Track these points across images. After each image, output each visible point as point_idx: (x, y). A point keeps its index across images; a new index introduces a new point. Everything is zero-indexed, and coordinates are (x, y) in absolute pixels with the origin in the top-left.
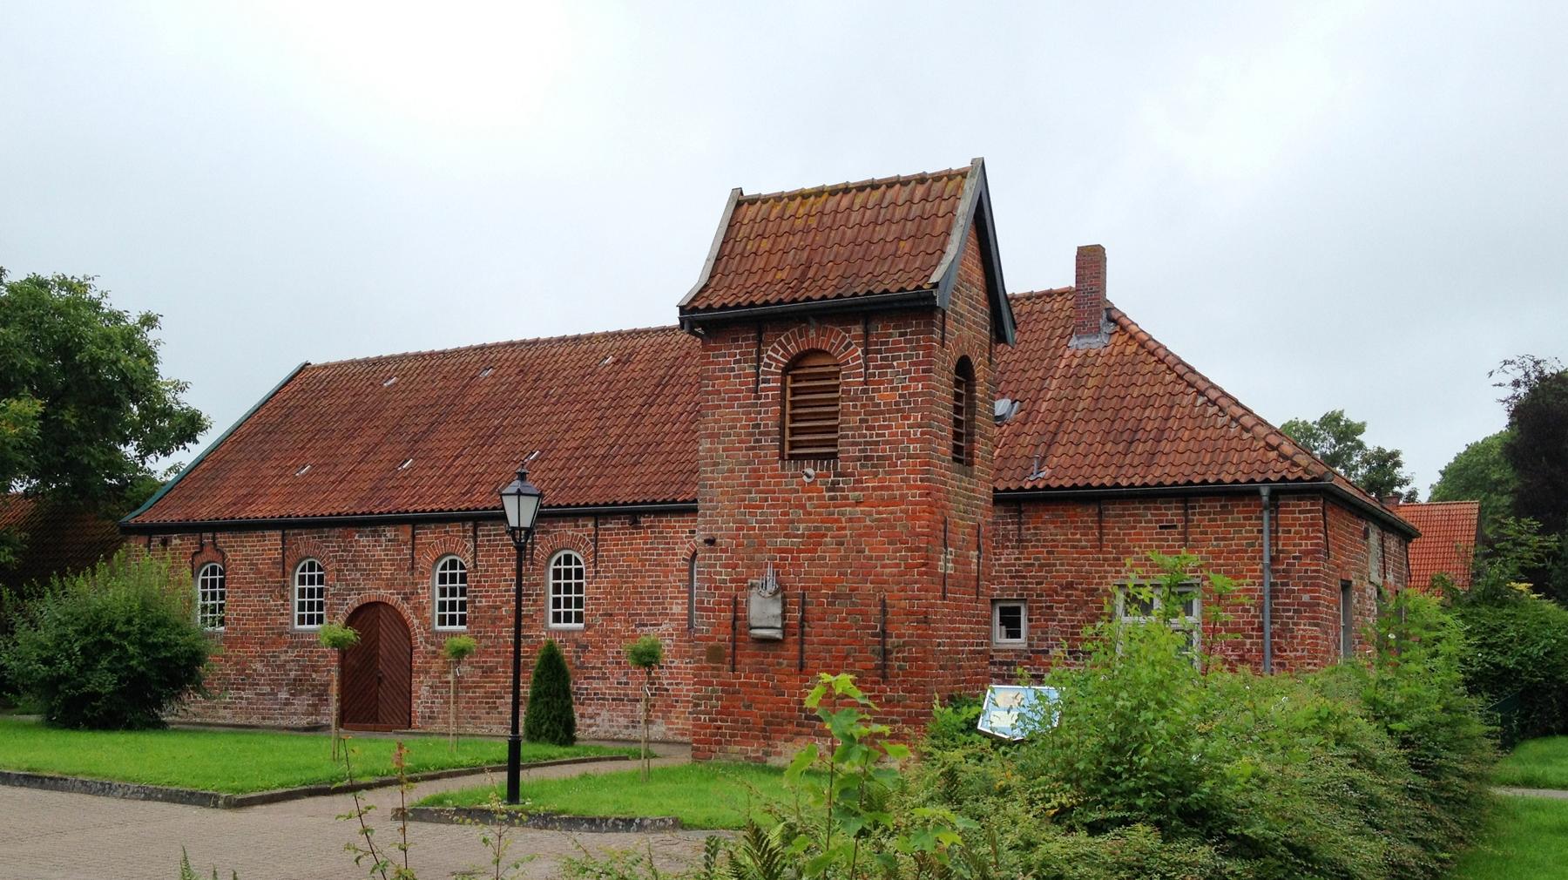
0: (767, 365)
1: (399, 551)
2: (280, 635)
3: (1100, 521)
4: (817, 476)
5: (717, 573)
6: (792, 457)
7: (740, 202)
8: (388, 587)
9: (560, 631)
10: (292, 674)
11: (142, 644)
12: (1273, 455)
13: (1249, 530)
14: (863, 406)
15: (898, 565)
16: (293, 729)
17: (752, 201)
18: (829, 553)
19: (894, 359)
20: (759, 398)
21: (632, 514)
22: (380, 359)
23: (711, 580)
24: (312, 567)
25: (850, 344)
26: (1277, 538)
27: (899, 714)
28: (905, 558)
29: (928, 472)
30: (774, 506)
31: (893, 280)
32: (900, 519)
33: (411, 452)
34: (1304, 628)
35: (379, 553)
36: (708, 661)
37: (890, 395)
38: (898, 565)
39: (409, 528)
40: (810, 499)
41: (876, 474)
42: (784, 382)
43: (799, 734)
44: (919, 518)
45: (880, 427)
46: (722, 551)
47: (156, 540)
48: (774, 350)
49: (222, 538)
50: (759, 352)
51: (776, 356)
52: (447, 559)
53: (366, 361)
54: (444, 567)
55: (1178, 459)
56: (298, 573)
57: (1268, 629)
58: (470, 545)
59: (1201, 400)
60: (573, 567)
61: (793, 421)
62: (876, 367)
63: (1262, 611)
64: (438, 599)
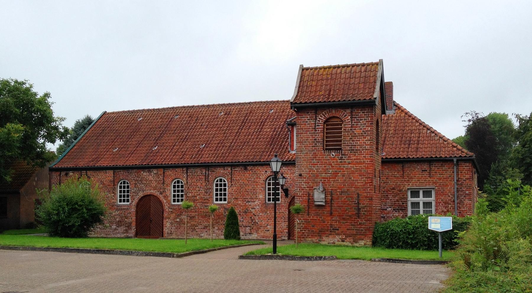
0: (319, 121)
1: (158, 178)
2: (113, 206)
3: (403, 169)
4: (336, 155)
6: (326, 149)
7: (303, 70)
8: (154, 190)
9: (218, 204)
10: (118, 219)
11: (87, 209)
12: (455, 149)
13: (449, 172)
14: (351, 134)
15: (362, 183)
16: (119, 238)
17: (307, 69)
18: (340, 179)
19: (361, 120)
20: (316, 131)
21: (245, 166)
22: (134, 111)
23: (300, 187)
24: (124, 183)
25: (346, 115)
26: (458, 174)
27: (363, 228)
28: (365, 180)
29: (372, 154)
30: (321, 164)
31: (360, 96)
32: (363, 169)
33: (156, 144)
34: (467, 201)
35: (150, 178)
37: (357, 130)
38: (362, 183)
39: (162, 170)
40: (333, 162)
41: (355, 155)
42: (324, 126)
43: (330, 234)
44: (370, 168)
45: (356, 141)
47: (63, 173)
48: (321, 116)
49: (89, 173)
50: (316, 117)
51: (321, 118)
52: (176, 180)
53: (129, 111)
54: (175, 183)
55: (426, 150)
56: (119, 185)
57: (456, 201)
58: (185, 175)
59: (428, 132)
60: (223, 183)
61: (326, 138)
62: (355, 122)
63: (454, 196)
64: (173, 193)
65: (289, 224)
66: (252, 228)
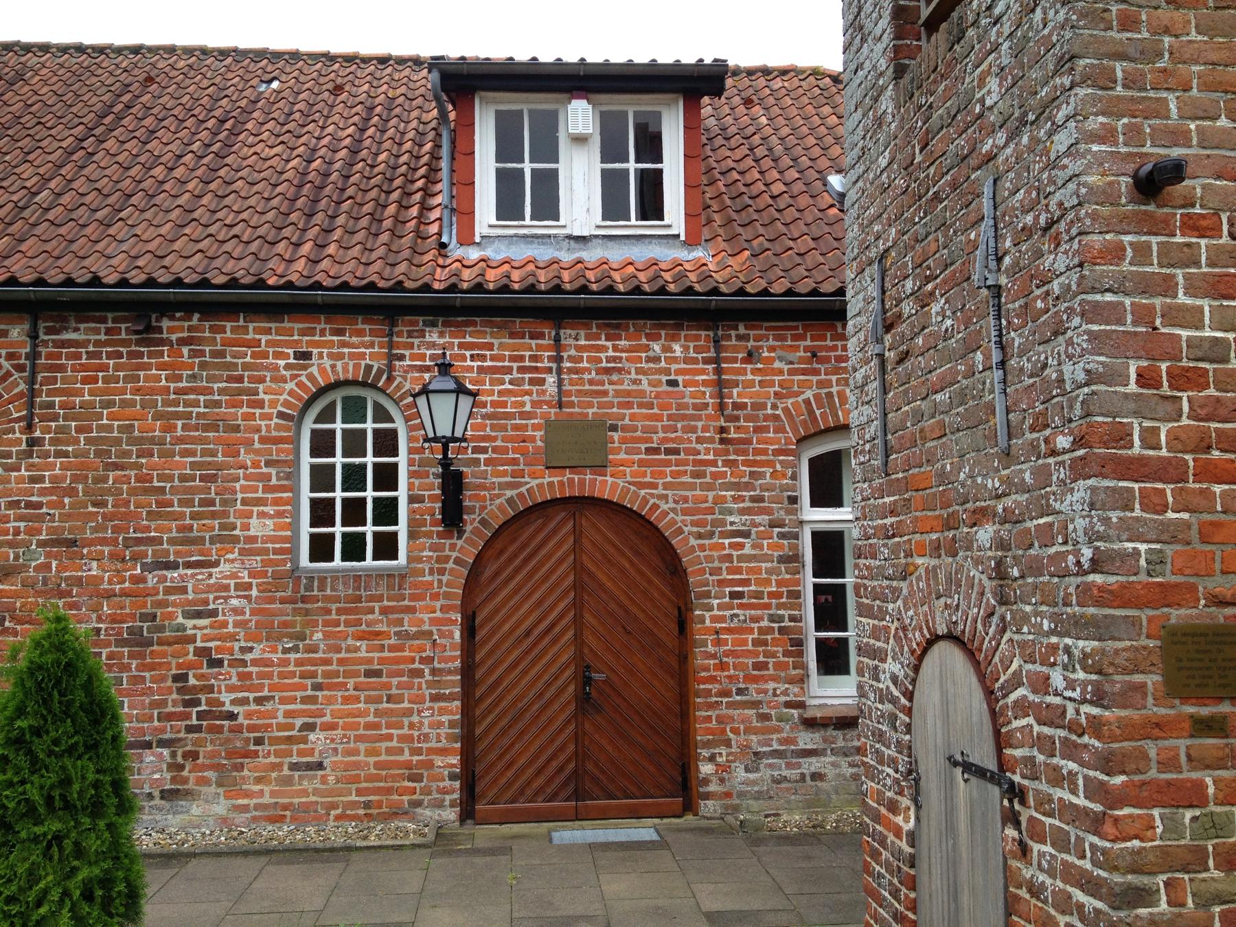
5: (1177, 316)
21: (142, 309)
23: (1154, 346)
36: (1175, 689)
46: (1193, 226)
65: (466, 711)
66: (193, 755)
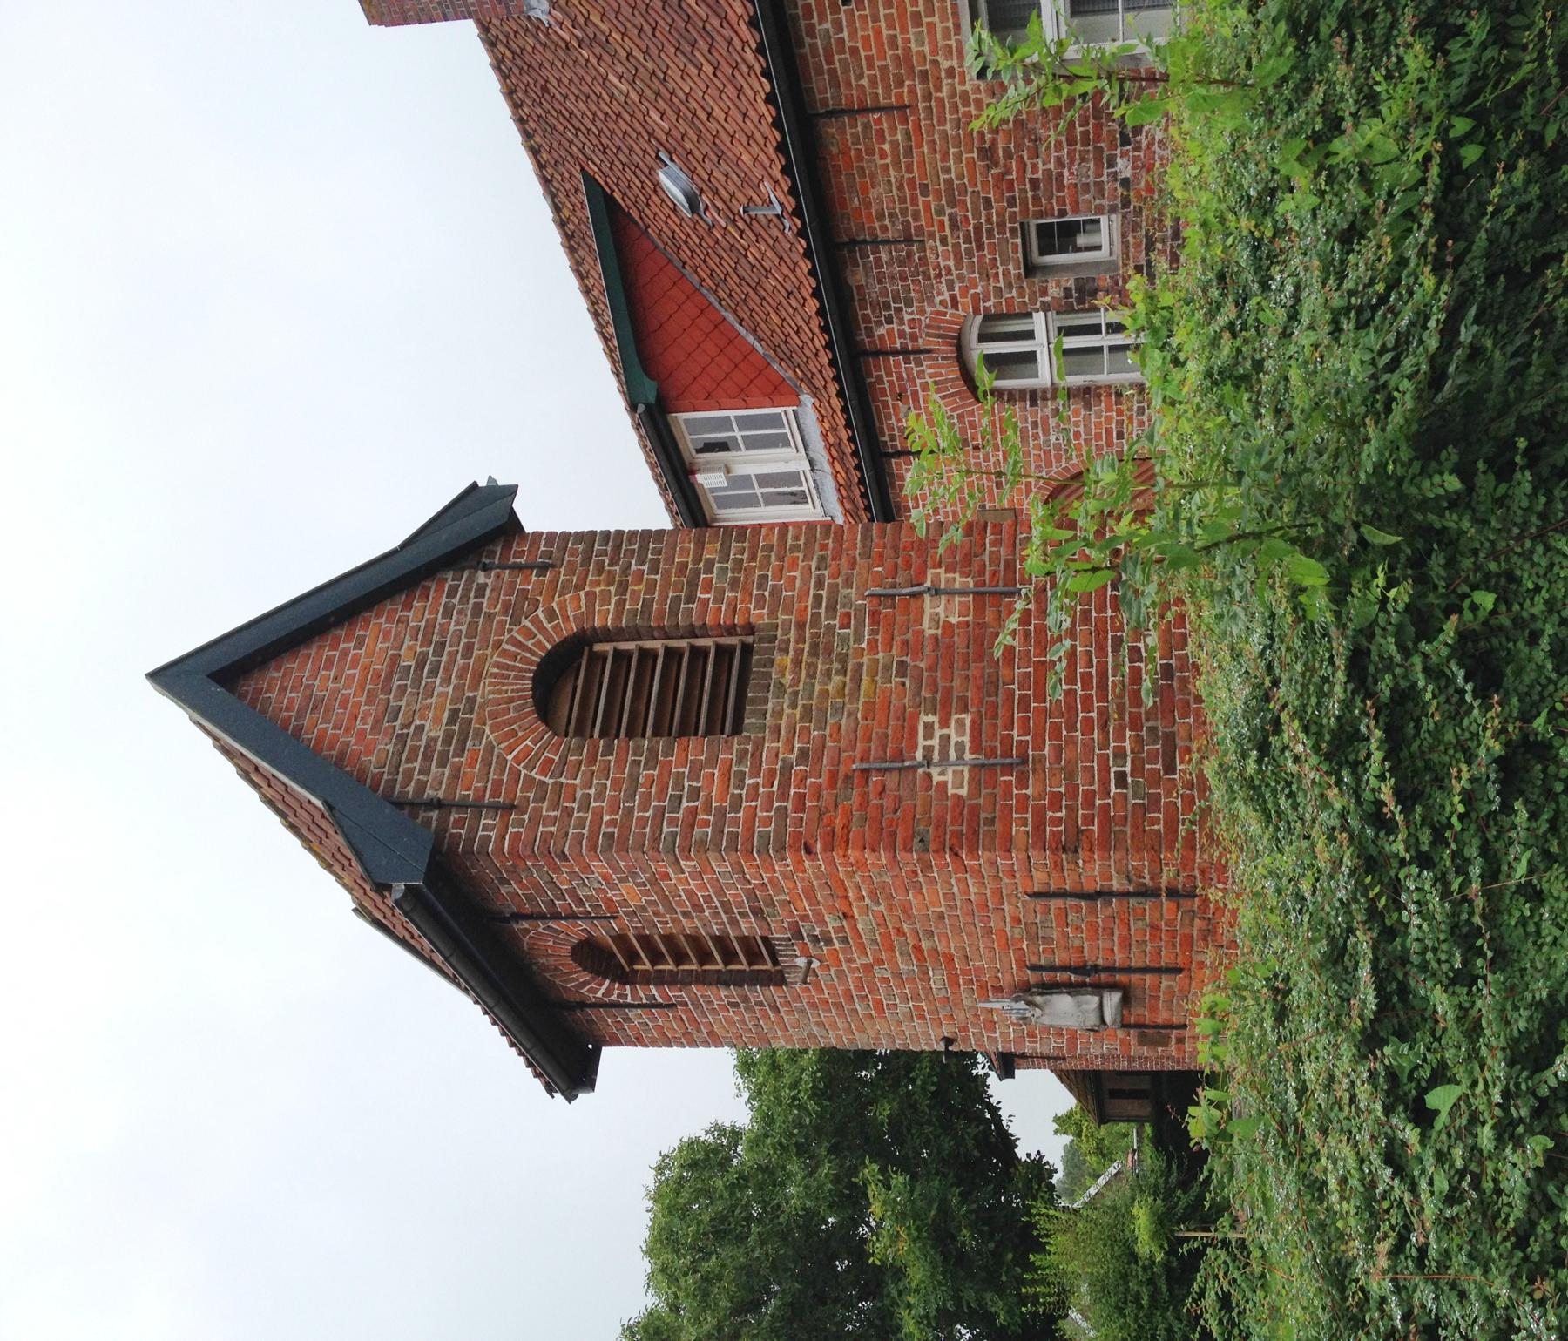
3: (851, 112)
